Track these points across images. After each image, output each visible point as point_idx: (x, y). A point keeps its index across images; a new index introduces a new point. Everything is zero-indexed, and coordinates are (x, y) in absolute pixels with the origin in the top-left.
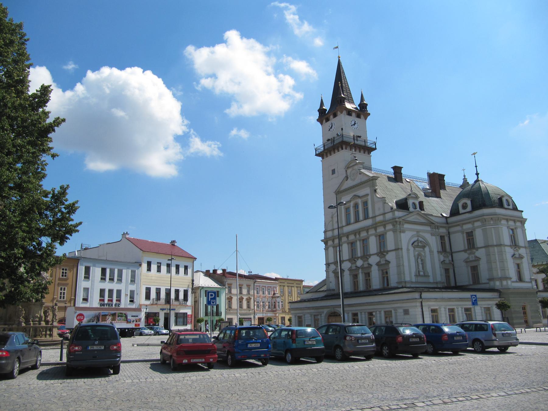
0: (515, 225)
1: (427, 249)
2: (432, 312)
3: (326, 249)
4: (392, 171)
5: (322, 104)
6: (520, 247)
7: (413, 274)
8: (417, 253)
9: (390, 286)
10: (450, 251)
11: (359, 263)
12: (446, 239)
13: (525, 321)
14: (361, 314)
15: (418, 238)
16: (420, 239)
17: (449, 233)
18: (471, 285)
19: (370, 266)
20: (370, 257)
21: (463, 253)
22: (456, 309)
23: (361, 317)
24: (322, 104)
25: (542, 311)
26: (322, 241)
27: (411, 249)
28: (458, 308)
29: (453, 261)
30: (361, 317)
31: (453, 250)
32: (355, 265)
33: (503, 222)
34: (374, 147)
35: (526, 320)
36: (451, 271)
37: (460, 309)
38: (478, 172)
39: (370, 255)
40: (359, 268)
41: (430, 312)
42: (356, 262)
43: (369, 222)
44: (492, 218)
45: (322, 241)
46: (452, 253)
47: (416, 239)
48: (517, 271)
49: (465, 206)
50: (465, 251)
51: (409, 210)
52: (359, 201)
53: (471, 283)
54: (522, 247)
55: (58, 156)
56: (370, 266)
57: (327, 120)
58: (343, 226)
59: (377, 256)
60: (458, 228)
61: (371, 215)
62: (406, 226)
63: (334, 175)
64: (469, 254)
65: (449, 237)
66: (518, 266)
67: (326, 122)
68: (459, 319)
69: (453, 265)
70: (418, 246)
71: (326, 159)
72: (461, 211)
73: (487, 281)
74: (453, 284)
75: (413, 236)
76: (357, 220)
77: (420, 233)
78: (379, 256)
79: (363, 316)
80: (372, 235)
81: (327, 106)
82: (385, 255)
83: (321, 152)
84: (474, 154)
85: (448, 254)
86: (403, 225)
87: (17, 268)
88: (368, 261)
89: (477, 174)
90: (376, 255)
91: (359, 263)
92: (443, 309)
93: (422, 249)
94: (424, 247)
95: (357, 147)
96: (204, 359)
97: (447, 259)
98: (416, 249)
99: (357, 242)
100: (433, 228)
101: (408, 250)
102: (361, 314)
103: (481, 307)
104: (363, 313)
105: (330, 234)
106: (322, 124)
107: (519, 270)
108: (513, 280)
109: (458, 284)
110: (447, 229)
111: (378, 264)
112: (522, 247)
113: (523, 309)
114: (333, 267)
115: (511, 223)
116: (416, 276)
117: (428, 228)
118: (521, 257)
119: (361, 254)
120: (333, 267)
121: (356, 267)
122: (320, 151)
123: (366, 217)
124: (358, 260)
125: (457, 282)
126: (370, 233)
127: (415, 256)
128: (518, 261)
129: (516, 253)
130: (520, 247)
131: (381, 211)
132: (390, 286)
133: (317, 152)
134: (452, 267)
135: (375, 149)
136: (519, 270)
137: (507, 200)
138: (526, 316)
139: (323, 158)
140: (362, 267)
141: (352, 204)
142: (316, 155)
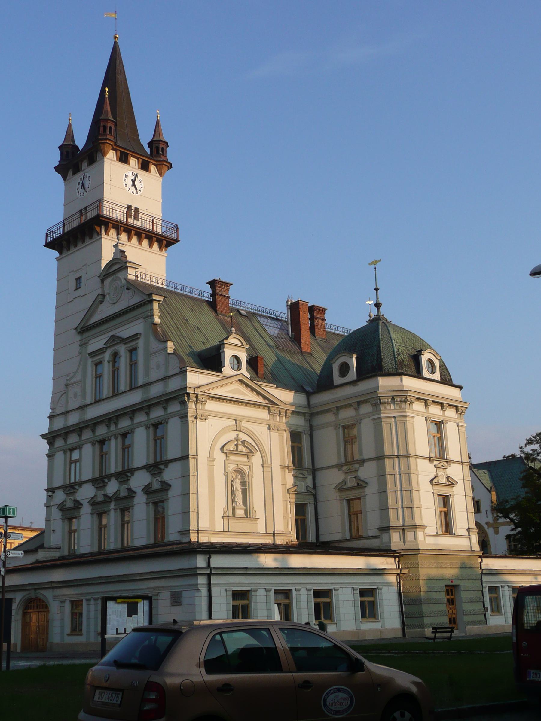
0: (444, 415)
1: (257, 459)
2: (233, 599)
3: (50, 456)
4: (208, 289)
5: (69, 135)
6: (449, 462)
7: (219, 513)
8: (231, 467)
9: (166, 540)
10: (311, 467)
11: (112, 487)
12: (305, 439)
13: (450, 619)
14: (88, 605)
15: (237, 435)
16: (243, 437)
17: (311, 427)
18: (345, 540)
19: (131, 493)
20: (132, 474)
21: (335, 470)
22: (294, 593)
23: (89, 611)
24: (69, 135)
25: (491, 599)
26: (44, 436)
27: (220, 457)
28: (299, 590)
29: (315, 487)
30: (89, 611)
31: (317, 466)
32: (103, 492)
33: (418, 406)
34: (174, 236)
35: (453, 616)
36: (310, 510)
37: (303, 592)
38: (380, 301)
39: (132, 471)
40: (110, 498)
41: (230, 598)
42: (161, 473)
43: (135, 398)
44: (393, 397)
45: (44, 436)
46: (314, 471)
47: (232, 435)
48: (440, 511)
49: (344, 369)
50: (339, 466)
51: (221, 372)
52: (122, 349)
53: (348, 537)
54: (457, 462)
55: (75, 290)
56: (131, 493)
57: (77, 170)
58: (87, 406)
59: (147, 472)
60: (329, 418)
61: (141, 381)
62: (211, 406)
63: (80, 292)
64: (345, 473)
65: (311, 436)
66: (446, 500)
67: (74, 173)
68: (299, 615)
69: (315, 496)
70: (236, 453)
71: (65, 253)
72: (337, 380)
73: (377, 533)
74: (312, 538)
75: (224, 430)
76: (115, 394)
77: (244, 424)
78: (150, 472)
79: (92, 607)
80: (140, 425)
81: (81, 141)
82: (161, 472)
83: (57, 239)
84: (374, 263)
85: (306, 473)
86: (204, 402)
87: (531, 532)
88: (129, 485)
89: (378, 305)
90: (145, 470)
91: (112, 487)
92: (261, 593)
93: (245, 459)
94: (249, 454)
95: (133, 232)
96: (380, 690)
97: (303, 483)
98: (232, 458)
99: (110, 439)
100: (274, 414)
101: (211, 459)
102: (88, 605)
103: (353, 589)
104: (92, 602)
105: (59, 424)
106: (65, 178)
107: (445, 510)
108: (428, 531)
109: (324, 538)
110: (308, 418)
111: (147, 490)
112: (457, 462)
113: (448, 594)
114: (60, 496)
115: (435, 410)
116: (226, 517)
117: (263, 414)
118: (451, 483)
119: (116, 467)
120: (60, 496)
121: (105, 495)
122: (56, 236)
123: (132, 388)
124: (109, 480)
125: (320, 533)
126: (84, 437)
127: (226, 474)
128: (445, 491)
129: (439, 474)
130: (449, 462)
131: (161, 374)
132: (166, 540)
133: (50, 239)
134: (312, 501)
135: (177, 241)
136: (445, 510)
137: (430, 361)
138: (455, 608)
139: (61, 253)
140: (116, 498)
141: (107, 356)
142: (48, 245)
